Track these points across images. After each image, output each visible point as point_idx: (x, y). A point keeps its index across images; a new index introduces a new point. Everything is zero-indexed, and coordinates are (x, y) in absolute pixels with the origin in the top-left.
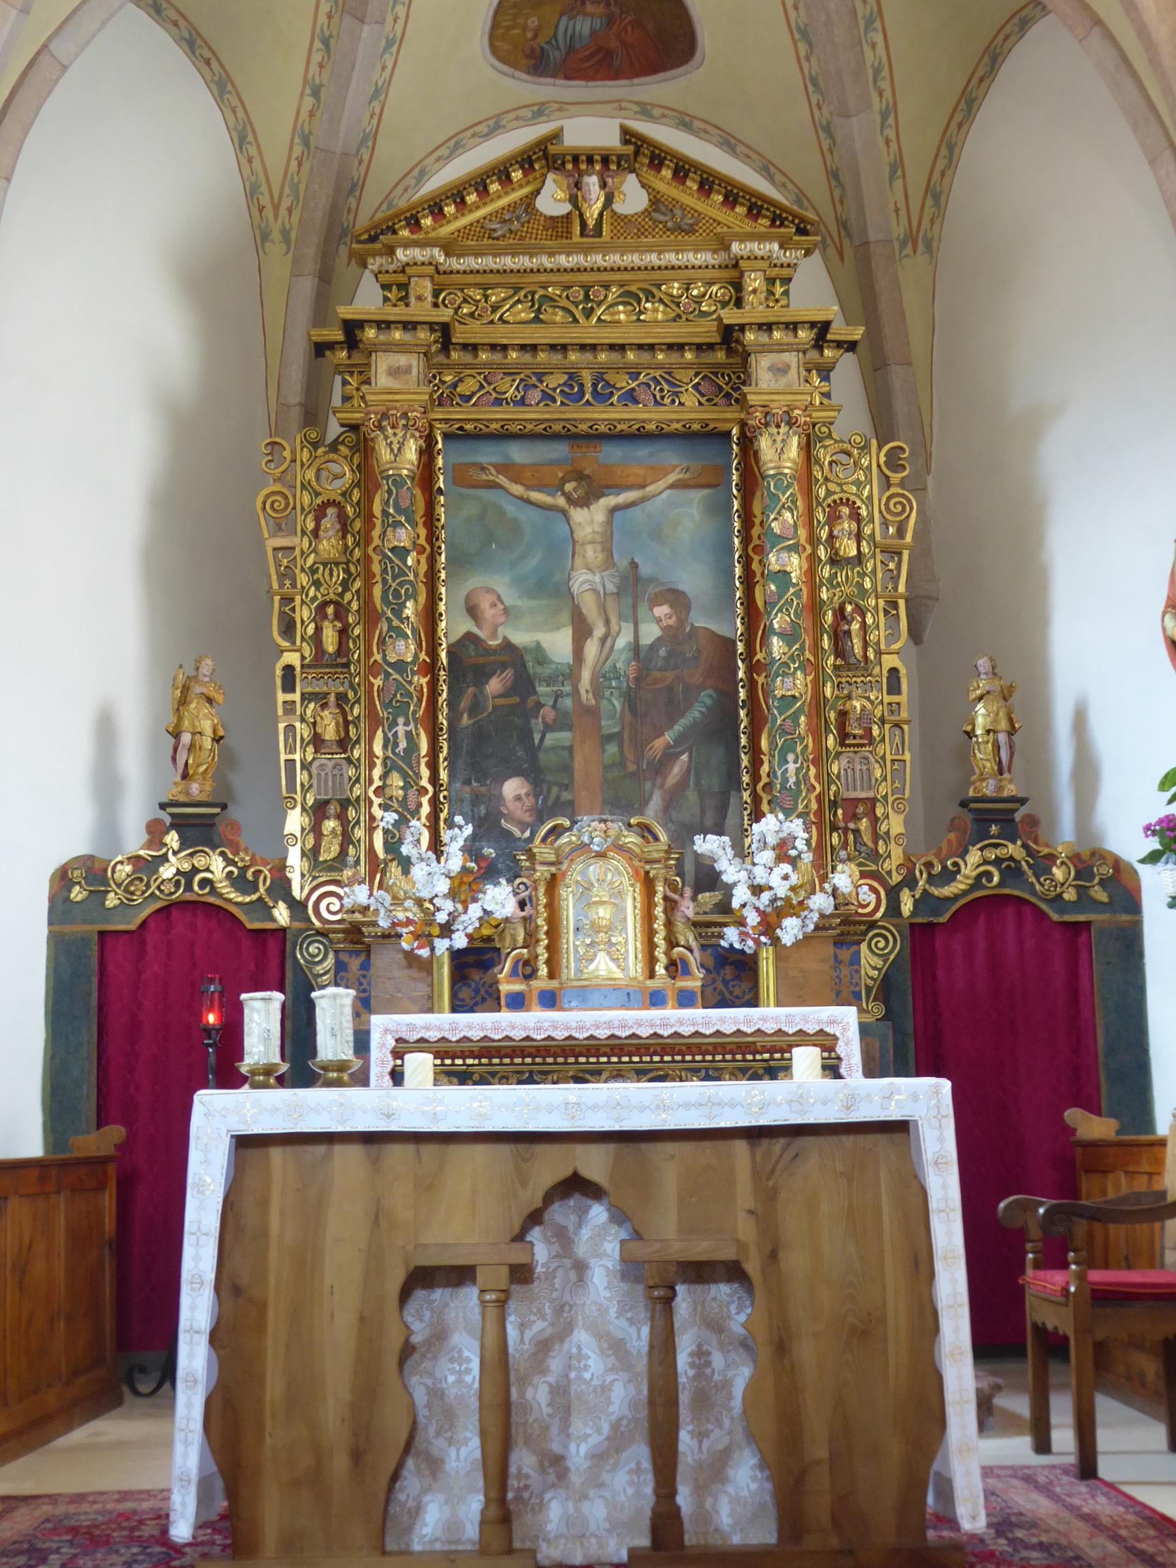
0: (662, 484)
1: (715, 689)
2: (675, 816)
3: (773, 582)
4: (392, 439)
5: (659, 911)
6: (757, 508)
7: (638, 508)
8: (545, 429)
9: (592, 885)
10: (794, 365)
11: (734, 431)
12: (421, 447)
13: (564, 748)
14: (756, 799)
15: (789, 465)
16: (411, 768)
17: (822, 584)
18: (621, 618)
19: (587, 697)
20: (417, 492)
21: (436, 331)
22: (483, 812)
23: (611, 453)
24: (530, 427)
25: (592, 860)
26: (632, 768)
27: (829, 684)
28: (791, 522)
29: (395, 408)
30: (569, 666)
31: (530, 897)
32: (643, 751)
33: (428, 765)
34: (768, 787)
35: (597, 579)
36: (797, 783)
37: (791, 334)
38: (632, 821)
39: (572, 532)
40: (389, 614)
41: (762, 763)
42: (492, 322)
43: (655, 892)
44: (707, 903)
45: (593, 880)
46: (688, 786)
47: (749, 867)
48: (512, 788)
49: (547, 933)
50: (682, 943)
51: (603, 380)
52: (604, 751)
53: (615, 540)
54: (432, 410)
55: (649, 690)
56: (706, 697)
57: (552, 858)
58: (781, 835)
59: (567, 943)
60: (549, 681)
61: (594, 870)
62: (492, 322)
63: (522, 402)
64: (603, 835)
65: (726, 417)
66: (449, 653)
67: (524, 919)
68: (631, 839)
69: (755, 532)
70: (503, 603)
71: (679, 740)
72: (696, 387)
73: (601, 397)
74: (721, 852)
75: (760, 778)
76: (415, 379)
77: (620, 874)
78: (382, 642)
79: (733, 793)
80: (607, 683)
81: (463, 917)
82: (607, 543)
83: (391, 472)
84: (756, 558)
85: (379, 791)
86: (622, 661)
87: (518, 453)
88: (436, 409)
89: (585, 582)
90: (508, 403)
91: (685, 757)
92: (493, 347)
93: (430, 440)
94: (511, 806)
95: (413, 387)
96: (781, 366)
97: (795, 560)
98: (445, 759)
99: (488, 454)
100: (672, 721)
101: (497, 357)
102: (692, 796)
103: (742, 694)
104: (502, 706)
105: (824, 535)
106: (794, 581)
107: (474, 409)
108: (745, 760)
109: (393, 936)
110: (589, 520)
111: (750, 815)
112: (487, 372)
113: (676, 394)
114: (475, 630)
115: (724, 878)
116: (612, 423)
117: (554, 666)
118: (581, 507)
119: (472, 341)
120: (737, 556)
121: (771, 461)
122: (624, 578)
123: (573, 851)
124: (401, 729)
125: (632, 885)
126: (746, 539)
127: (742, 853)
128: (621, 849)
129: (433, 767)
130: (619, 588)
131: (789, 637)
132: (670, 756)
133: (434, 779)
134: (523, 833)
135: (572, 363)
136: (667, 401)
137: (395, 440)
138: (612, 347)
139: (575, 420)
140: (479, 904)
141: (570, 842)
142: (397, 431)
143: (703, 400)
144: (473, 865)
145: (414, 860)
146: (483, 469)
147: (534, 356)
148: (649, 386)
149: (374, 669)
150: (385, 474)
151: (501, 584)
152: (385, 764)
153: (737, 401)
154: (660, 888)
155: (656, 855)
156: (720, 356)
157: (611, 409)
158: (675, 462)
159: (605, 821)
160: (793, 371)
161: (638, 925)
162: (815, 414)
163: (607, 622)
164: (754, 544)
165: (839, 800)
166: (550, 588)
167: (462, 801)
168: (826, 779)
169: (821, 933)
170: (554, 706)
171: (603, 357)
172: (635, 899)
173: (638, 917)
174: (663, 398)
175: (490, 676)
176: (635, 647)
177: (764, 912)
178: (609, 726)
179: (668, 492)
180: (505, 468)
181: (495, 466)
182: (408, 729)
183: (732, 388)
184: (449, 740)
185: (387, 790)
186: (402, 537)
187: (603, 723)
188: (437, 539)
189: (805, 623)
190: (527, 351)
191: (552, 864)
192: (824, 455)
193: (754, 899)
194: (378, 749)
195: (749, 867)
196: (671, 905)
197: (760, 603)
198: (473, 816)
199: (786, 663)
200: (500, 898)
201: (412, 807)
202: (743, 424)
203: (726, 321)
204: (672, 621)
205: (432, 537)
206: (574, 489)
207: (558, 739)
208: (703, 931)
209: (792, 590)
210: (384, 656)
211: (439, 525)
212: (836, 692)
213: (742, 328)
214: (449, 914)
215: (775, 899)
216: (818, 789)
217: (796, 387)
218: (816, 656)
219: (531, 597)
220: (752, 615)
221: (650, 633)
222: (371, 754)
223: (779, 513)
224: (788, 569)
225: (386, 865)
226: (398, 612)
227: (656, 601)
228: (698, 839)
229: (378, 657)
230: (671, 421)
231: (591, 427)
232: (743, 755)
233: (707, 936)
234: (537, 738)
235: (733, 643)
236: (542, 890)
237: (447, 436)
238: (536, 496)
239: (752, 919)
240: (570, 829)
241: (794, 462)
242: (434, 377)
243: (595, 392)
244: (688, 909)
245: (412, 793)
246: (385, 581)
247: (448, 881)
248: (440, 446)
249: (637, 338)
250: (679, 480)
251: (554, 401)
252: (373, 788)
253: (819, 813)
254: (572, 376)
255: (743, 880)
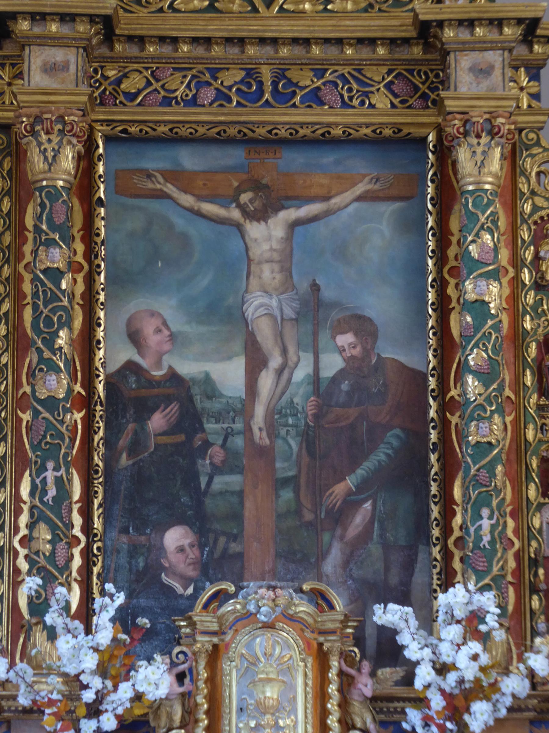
0: (348, 196)
1: (403, 429)
2: (356, 573)
3: (469, 312)
4: (46, 145)
5: (333, 689)
6: (454, 225)
7: (322, 222)
8: (219, 133)
9: (258, 659)
10: (498, 65)
11: (430, 138)
12: (79, 153)
13: (233, 493)
14: (447, 556)
15: (490, 179)
16: (61, 519)
17: (525, 312)
18: (299, 346)
19: (260, 436)
20: (76, 202)
21: (97, 23)
22: (142, 565)
23: (293, 160)
24: (201, 130)
25: (259, 632)
26: (308, 516)
27: (531, 426)
28: (491, 245)
29: (50, 112)
30: (241, 400)
31: (190, 670)
32: (321, 497)
33: (81, 512)
34: (460, 542)
35: (274, 303)
36: (492, 542)
37: (495, 30)
38: (305, 587)
39: (247, 249)
40: (40, 344)
41: (454, 513)
42: (161, 10)
43: (330, 667)
44: (387, 680)
45: (259, 654)
46: (372, 538)
47: (435, 642)
48: (175, 538)
49: (207, 713)
50: (359, 725)
51: (285, 77)
52: (278, 496)
53: (294, 261)
54: (93, 111)
55: (331, 431)
56: (393, 438)
57: (215, 627)
58: (471, 608)
59: (230, 724)
60: (218, 417)
61: (261, 642)
62: (161, 10)
63: (194, 102)
64: (271, 603)
65: (419, 120)
66: (108, 385)
67: (183, 695)
68: (303, 608)
69: (452, 252)
70: (168, 328)
71: (363, 487)
72: (388, 86)
73: (283, 97)
74: (403, 625)
75: (451, 531)
76: (73, 77)
77: (289, 647)
78: (31, 374)
79: (421, 547)
80: (283, 421)
81: (113, 697)
82: (286, 262)
83: (44, 183)
84: (452, 282)
85: (25, 541)
86: (300, 395)
87: (189, 159)
88: (97, 109)
89: (261, 305)
90: (177, 103)
91: (368, 505)
92: (162, 40)
93: (90, 145)
94: (173, 558)
95: (71, 86)
96: (483, 67)
97: (494, 288)
98: (100, 506)
99: (154, 160)
100: (352, 470)
101: (167, 50)
102: (375, 549)
103: (433, 436)
104: (166, 445)
105: (529, 256)
106: (493, 312)
107: (140, 109)
108: (435, 511)
109: (35, 712)
110: (266, 236)
111: (439, 573)
112: (155, 66)
113: (366, 94)
114: (137, 358)
115: (406, 653)
116: (293, 127)
117: (224, 400)
118: (258, 220)
119: (139, 33)
120: (430, 280)
121: (470, 175)
122: (304, 303)
123: (237, 620)
124: (50, 475)
125: (303, 660)
126: (441, 259)
127: (428, 622)
128: (292, 619)
129: (86, 513)
130: (298, 313)
131: (486, 376)
132: (351, 504)
133: (87, 528)
134: (186, 588)
135: (251, 58)
136: (356, 102)
137: (49, 147)
138: (295, 41)
139: (253, 123)
140: (130, 683)
141: (234, 611)
142: (52, 137)
143: (396, 101)
144: (124, 637)
145: (59, 630)
146: (149, 176)
147: (208, 50)
148: (336, 85)
149: (22, 403)
150: (38, 185)
151: (168, 307)
152: (32, 515)
153: (434, 102)
154: (335, 663)
155: (330, 626)
156: (417, 51)
157: (293, 111)
158: (363, 171)
159: (274, 588)
160: (497, 72)
161: (309, 706)
162: (520, 119)
163: (284, 352)
164: (450, 266)
165: (540, 559)
166: (223, 315)
167: (118, 552)
168: (526, 533)
169: (516, 715)
170: (223, 446)
171: (284, 51)
172: (306, 675)
173: (310, 696)
174: (351, 98)
175: (153, 410)
176: (315, 379)
177: (451, 695)
178: (283, 468)
179: (355, 205)
180: (175, 176)
181: (163, 173)
182: (59, 474)
183: (429, 88)
184: (105, 484)
185: (33, 543)
186: (56, 257)
187: (278, 465)
188: (96, 257)
189: (506, 356)
190: (199, 44)
191: (214, 633)
192: (531, 166)
193: (439, 680)
194: (25, 491)
195: (435, 642)
196: (347, 682)
197: (455, 332)
198: (130, 570)
199: (481, 405)
200: (154, 678)
201: (61, 562)
202: (440, 130)
203: (422, 17)
204: (357, 352)
205: (90, 254)
206: (251, 201)
207: (227, 483)
208: (384, 705)
209: (490, 323)
210: (34, 391)
211: (99, 240)
212: (539, 435)
213: (441, 24)
214: (97, 693)
215: (461, 681)
216: (517, 544)
217: (499, 92)
218: (517, 393)
219: (201, 323)
220: (446, 346)
221: (332, 364)
222: (17, 498)
223: (477, 235)
224: (486, 299)
225: (30, 628)
226: (50, 342)
227: (340, 328)
228: (378, 609)
229: (27, 389)
230: (360, 125)
231: (270, 132)
232: (433, 506)
233: (389, 711)
234: (203, 481)
235: (424, 377)
236: (202, 664)
237: (108, 139)
238: (208, 208)
239: (437, 702)
240: (235, 595)
241: (496, 176)
242: (96, 71)
243: (275, 91)
244: (366, 686)
245: (61, 546)
246: (35, 307)
247: (96, 656)
248: (101, 150)
249: (322, 32)
250: (367, 192)
251: (230, 101)
252: (18, 538)
253: (518, 572)
254: (249, 73)
255: (427, 659)
